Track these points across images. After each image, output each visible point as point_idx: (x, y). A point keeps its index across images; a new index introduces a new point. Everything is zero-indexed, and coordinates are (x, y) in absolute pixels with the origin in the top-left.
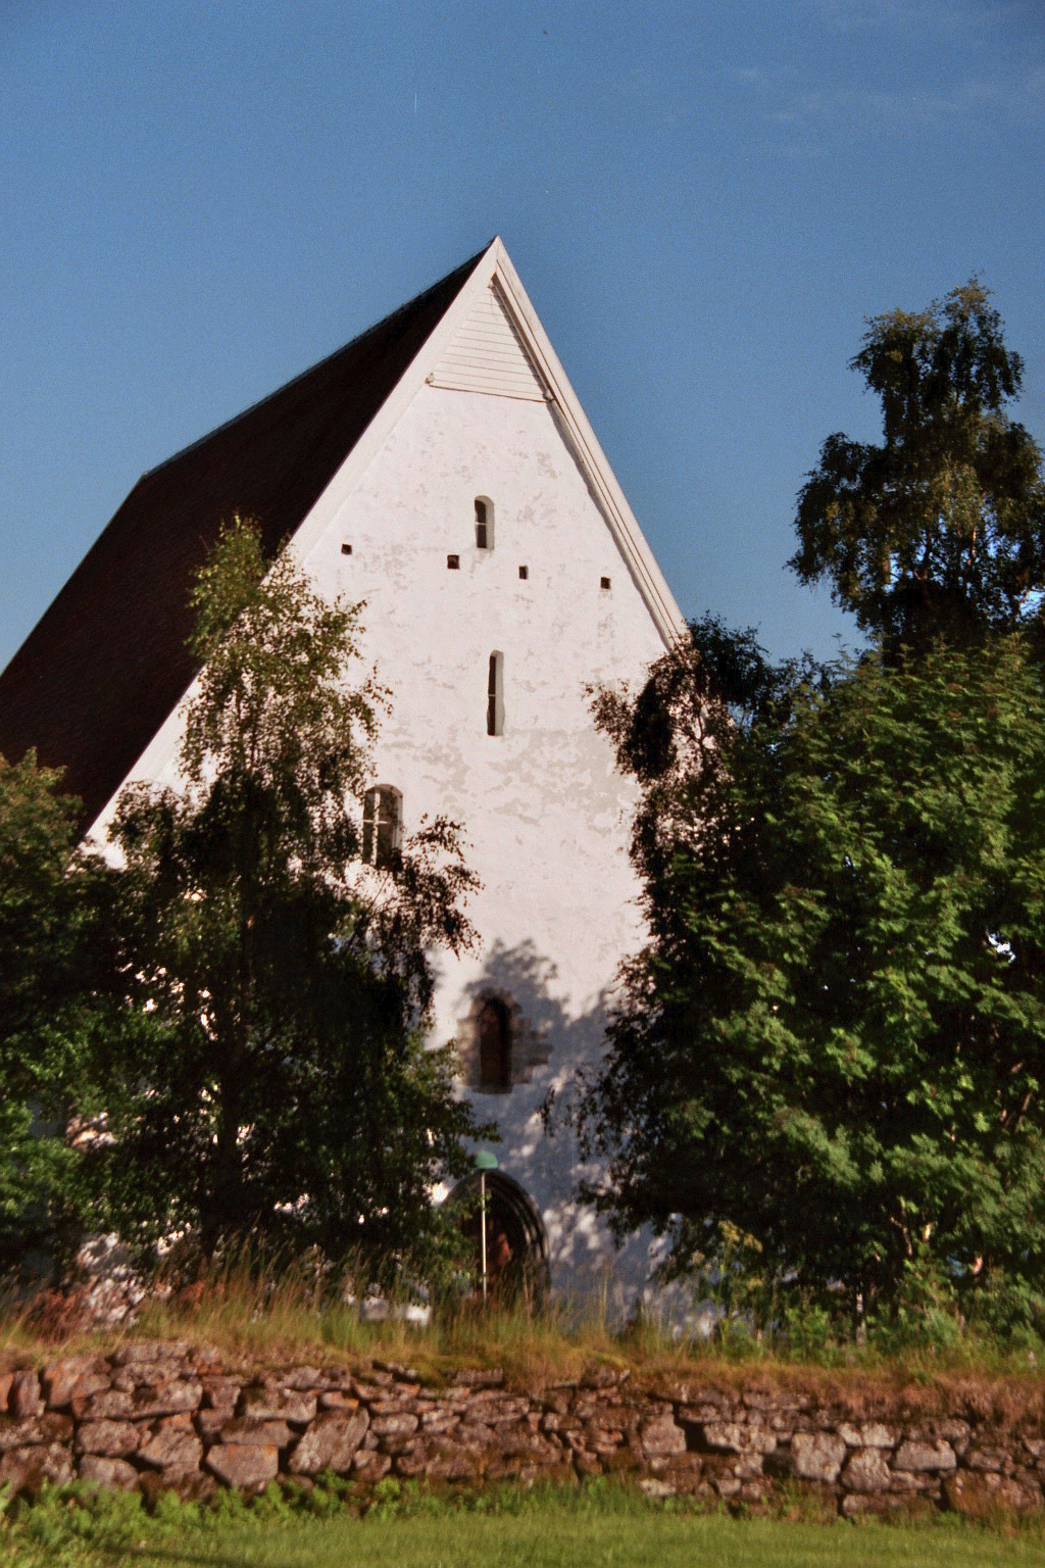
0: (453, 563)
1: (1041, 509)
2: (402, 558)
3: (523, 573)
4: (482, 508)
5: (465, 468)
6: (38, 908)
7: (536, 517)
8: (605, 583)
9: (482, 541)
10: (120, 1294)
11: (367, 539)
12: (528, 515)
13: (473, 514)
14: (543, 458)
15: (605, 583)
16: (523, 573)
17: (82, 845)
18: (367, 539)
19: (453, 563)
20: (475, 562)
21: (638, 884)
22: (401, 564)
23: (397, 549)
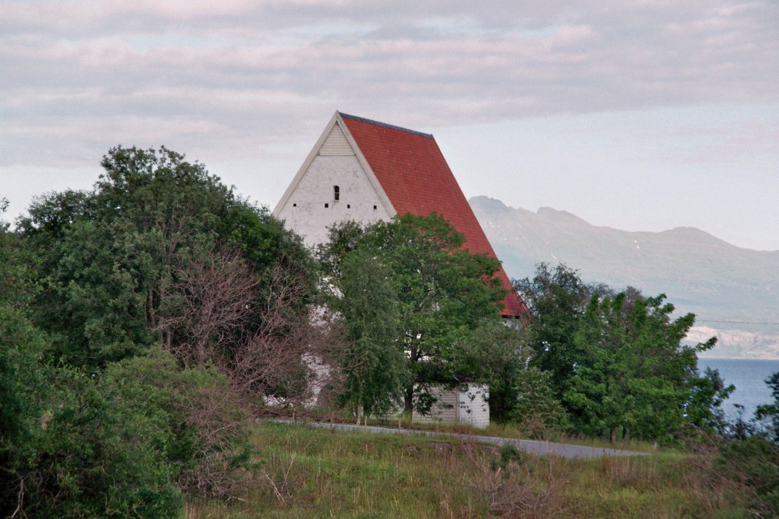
0: (327, 206)
1: (2, 371)
2: (311, 206)
3: (349, 207)
4: (337, 189)
5: (330, 178)
6: (120, 216)
7: (353, 190)
8: (375, 207)
9: (337, 198)
10: (243, 361)
11: (300, 201)
12: (350, 189)
13: (332, 191)
14: (355, 172)
15: (375, 207)
16: (349, 207)
17: (584, 435)
18: (300, 201)
19: (327, 206)
20: (333, 205)
21: (672, 228)
22: (310, 208)
23: (309, 204)
